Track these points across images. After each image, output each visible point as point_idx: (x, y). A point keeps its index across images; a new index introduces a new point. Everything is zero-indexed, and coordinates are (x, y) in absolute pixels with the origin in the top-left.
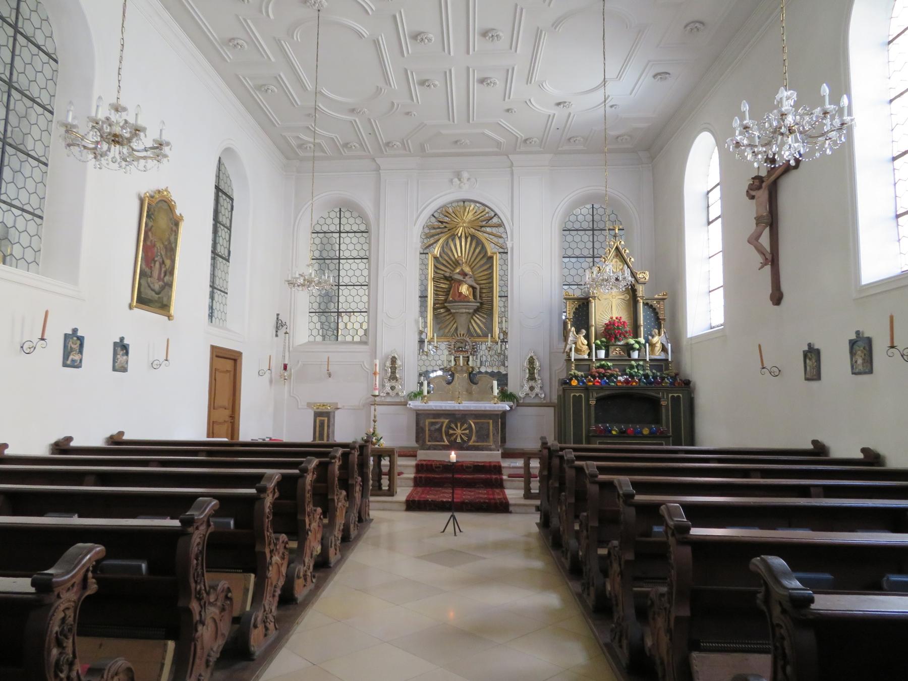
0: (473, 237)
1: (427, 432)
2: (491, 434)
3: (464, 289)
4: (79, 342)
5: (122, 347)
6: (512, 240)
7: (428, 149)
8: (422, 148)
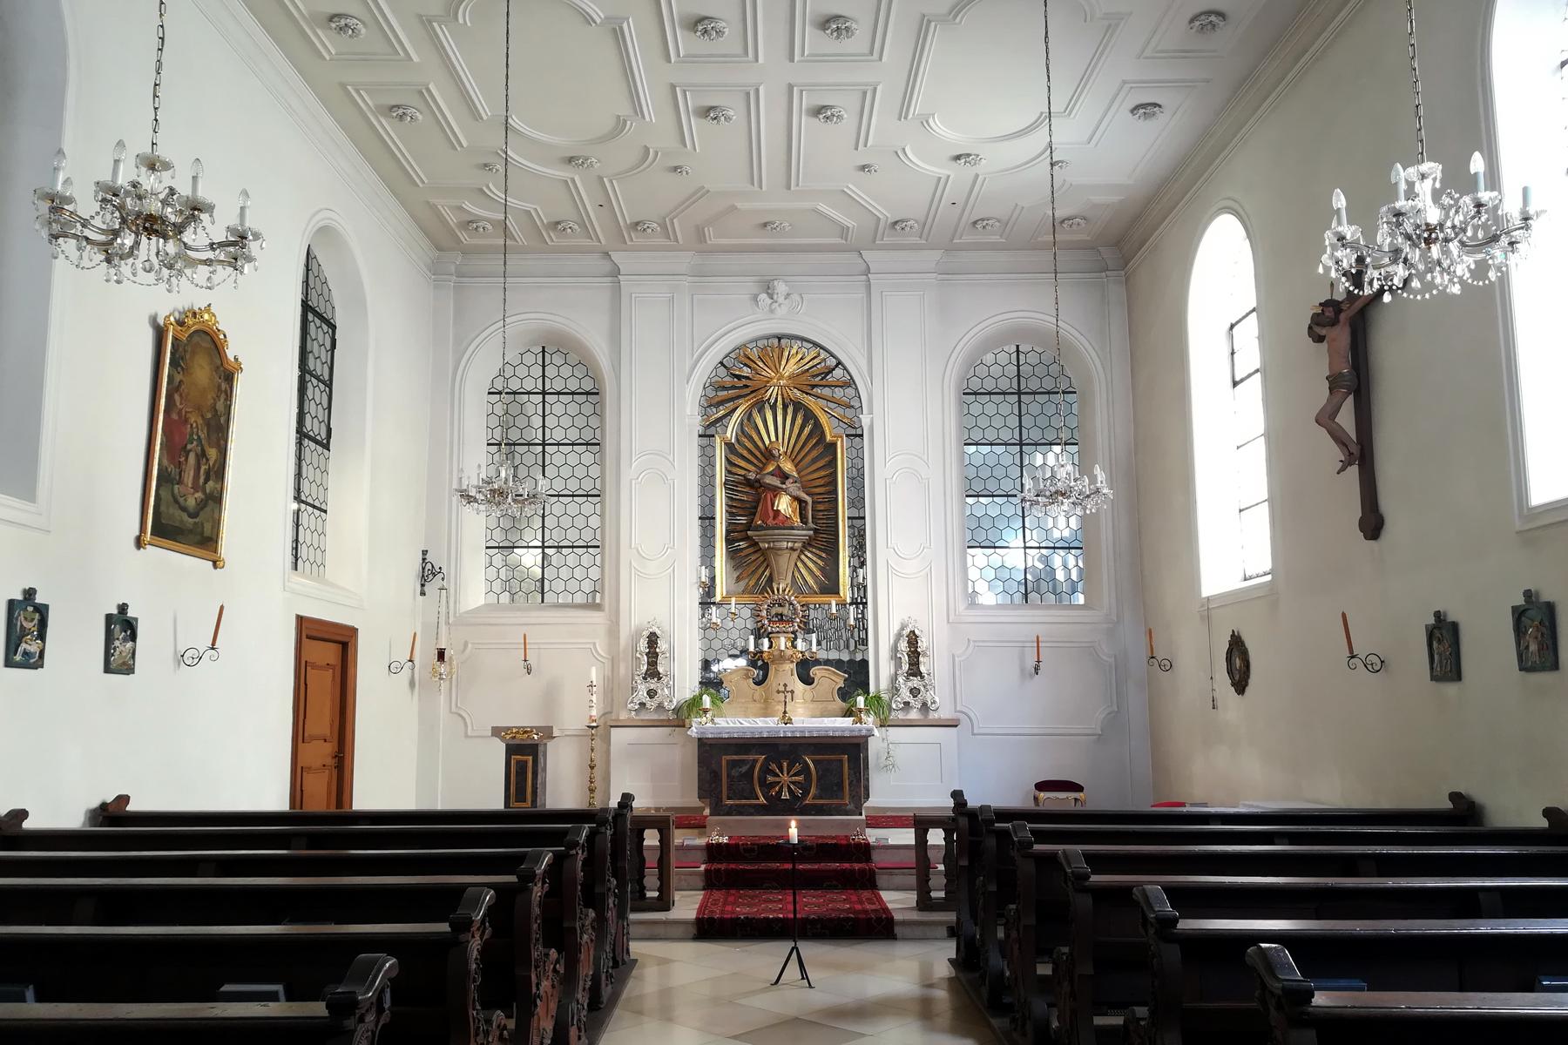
0: (798, 406)
3: (784, 505)
4: (37, 616)
5: (121, 625)
7: (704, 239)
8: (700, 235)
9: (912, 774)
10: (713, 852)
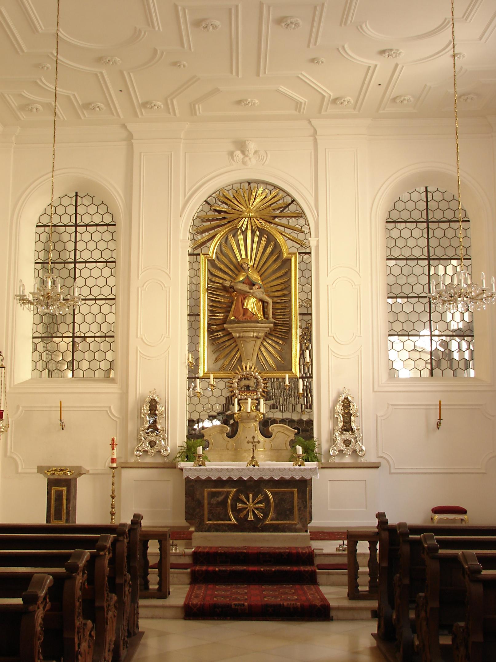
0: (262, 232)
1: (206, 506)
2: (296, 509)
3: (251, 304)
6: (317, 235)
9: (344, 502)
10: (199, 557)
